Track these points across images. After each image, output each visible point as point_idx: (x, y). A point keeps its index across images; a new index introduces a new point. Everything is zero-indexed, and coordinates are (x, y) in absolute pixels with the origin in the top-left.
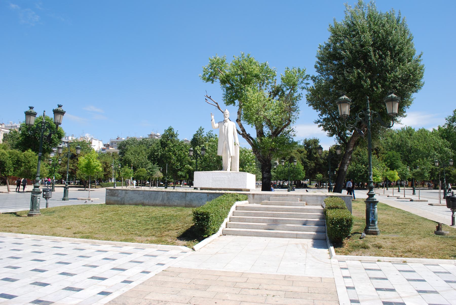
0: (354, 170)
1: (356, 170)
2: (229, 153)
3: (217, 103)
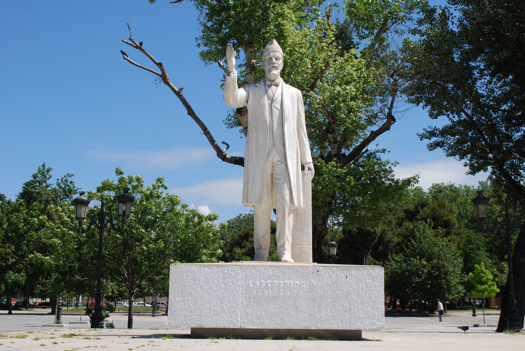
0: (403, 272)
1: (407, 271)
2: (287, 197)
3: (160, 65)
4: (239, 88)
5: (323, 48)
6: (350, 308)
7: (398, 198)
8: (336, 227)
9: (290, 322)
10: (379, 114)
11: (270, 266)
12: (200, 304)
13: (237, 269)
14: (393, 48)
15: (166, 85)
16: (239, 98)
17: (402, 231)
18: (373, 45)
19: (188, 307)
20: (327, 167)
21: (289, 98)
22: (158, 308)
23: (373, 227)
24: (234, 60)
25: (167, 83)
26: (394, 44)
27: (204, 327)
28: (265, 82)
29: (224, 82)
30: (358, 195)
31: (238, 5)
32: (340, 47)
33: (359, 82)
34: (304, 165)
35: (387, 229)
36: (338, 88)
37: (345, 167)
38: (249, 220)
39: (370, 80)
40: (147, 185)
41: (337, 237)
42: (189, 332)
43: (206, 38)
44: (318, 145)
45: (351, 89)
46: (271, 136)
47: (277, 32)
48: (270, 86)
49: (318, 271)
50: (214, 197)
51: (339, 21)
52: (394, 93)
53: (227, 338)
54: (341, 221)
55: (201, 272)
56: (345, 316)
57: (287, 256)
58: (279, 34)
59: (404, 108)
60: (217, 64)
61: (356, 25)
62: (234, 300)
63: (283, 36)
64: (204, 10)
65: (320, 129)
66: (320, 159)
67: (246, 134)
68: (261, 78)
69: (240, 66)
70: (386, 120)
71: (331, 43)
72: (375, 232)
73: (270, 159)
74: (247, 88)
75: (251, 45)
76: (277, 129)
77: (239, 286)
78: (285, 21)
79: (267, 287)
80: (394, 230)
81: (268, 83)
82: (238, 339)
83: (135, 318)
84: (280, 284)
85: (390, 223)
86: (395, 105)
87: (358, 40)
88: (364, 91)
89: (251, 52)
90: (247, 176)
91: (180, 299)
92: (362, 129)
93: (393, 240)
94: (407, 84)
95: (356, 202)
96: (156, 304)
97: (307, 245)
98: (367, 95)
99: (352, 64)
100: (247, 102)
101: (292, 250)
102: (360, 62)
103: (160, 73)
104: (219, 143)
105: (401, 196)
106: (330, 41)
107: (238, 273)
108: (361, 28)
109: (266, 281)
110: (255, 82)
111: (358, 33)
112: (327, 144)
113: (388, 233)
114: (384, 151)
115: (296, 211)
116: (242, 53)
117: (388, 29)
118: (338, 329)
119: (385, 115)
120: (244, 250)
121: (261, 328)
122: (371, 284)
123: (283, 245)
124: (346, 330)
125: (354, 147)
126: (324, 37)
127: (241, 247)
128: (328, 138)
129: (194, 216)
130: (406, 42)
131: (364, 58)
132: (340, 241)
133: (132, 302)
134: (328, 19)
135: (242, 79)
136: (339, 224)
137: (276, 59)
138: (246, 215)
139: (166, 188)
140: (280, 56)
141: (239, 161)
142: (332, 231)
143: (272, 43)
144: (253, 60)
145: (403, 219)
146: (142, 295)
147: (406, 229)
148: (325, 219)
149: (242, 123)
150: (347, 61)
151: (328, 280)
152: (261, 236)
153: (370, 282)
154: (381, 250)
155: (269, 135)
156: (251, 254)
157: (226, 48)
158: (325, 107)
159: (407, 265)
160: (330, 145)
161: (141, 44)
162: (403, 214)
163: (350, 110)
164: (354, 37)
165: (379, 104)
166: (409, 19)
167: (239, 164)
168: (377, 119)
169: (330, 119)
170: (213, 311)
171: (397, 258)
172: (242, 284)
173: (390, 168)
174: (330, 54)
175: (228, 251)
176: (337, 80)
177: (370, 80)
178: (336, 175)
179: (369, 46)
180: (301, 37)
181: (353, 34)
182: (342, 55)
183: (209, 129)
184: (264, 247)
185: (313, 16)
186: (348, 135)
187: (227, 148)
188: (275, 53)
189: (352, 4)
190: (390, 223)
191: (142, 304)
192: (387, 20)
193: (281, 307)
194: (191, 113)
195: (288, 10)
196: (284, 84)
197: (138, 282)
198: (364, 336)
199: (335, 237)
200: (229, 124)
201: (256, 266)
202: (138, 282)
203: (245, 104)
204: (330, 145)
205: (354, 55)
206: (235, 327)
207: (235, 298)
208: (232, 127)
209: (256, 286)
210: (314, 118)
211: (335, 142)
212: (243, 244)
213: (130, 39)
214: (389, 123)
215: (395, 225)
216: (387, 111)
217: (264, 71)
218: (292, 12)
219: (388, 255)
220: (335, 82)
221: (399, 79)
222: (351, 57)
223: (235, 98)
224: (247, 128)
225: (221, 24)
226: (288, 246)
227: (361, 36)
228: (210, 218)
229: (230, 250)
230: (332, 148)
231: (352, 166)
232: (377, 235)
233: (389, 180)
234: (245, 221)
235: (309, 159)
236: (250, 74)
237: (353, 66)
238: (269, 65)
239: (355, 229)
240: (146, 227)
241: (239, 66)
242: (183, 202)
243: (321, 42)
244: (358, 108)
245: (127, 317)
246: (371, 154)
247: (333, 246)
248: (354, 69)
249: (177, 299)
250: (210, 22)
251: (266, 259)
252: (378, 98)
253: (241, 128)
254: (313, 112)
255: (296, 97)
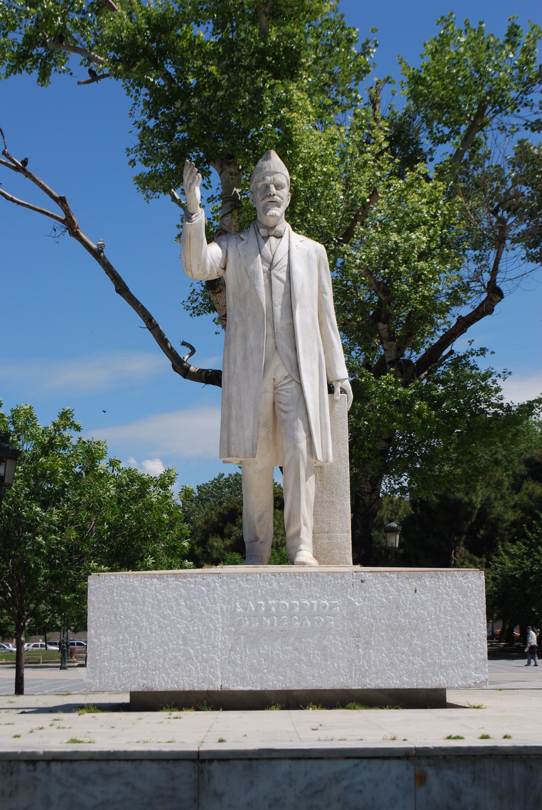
0: (526, 575)
1: (532, 573)
2: (303, 445)
3: (61, 201)
4: (208, 243)
5: (365, 163)
6: (424, 649)
7: (511, 439)
8: (397, 496)
9: (313, 676)
10: (472, 285)
11: (274, 574)
12: (145, 647)
13: (213, 580)
14: (496, 159)
15: (73, 240)
16: (209, 261)
17: (523, 500)
18: (459, 154)
19: (123, 653)
20: (378, 386)
21: (301, 259)
22: (72, 653)
23: (467, 494)
24: (198, 191)
25: (76, 235)
26: (497, 152)
27: (155, 689)
28: (257, 232)
29: (181, 230)
30: (437, 436)
31: (204, 85)
32: (397, 160)
33: (433, 225)
34: (334, 383)
35: (493, 496)
36: (394, 237)
37: (412, 385)
38: (235, 484)
39: (453, 220)
40: (45, 420)
41: (401, 512)
42: (126, 699)
43: (147, 149)
44: (360, 345)
45: (419, 237)
46: (271, 331)
47: (279, 134)
48: (266, 238)
49: (362, 581)
50: (171, 444)
51: (396, 111)
52: (499, 242)
53: (197, 709)
54: (405, 484)
55: (146, 587)
56: (414, 664)
57: (305, 554)
58: (283, 139)
59: (517, 273)
60: (169, 197)
61: (426, 116)
62: (209, 638)
63: (290, 142)
64: (141, 98)
65: (364, 313)
66: (364, 370)
67: (224, 327)
68: (250, 222)
69: (211, 199)
70: (485, 295)
71: (381, 153)
72: (470, 503)
73: (270, 375)
74: (224, 243)
75: (231, 161)
76: (282, 319)
77: (217, 612)
78: (295, 114)
79: (268, 613)
80: (507, 497)
81: (263, 232)
82: (218, 710)
83: (28, 674)
84: (292, 606)
85: (499, 484)
86: (501, 266)
87: (431, 146)
88: (444, 242)
89: (231, 174)
90: (227, 406)
91: (109, 639)
92: (442, 312)
93: (506, 516)
94: (524, 227)
95: (433, 448)
96: (68, 647)
97: (343, 532)
98: (447, 248)
99: (419, 191)
100: (225, 269)
101: (314, 542)
102: (435, 187)
103: (63, 217)
104: (175, 344)
105: (515, 435)
106: (378, 150)
107: (215, 589)
108: (435, 123)
109: (266, 601)
110: (241, 231)
111: (431, 132)
112: (377, 341)
113: (496, 504)
114: (483, 351)
115: (319, 471)
116: (215, 177)
117: (486, 123)
118: (403, 687)
119: (483, 285)
120: (228, 542)
121: (259, 689)
122: (462, 603)
123: (298, 534)
124: (416, 689)
125: (427, 346)
126: (368, 142)
127: (223, 536)
128: (377, 331)
129: (132, 481)
130: (523, 148)
131: (441, 180)
132: (406, 519)
133: (23, 644)
134: (375, 109)
135: (215, 223)
136: (403, 490)
137: (277, 187)
138: (230, 475)
139: (78, 429)
140: (285, 182)
141: (213, 378)
142: (391, 502)
143: (268, 158)
144: (235, 189)
145: (524, 477)
146: (41, 629)
147: (530, 496)
148: (376, 482)
149: (217, 307)
150: (410, 186)
151: (381, 596)
152: (256, 517)
153: (458, 599)
154: (483, 536)
155: (267, 330)
156: (239, 551)
157: (183, 166)
158: (370, 273)
159: (532, 563)
160: (381, 343)
161: (25, 162)
162: (523, 467)
163: (418, 277)
164: (424, 140)
165: (473, 266)
166: (526, 105)
167: (214, 384)
168: (469, 294)
169: (381, 295)
170: (171, 659)
171: (513, 549)
172: (222, 608)
173: (494, 382)
174: (378, 174)
175: (199, 544)
176: (392, 223)
177: (453, 220)
178: (395, 399)
179: (451, 155)
180: (324, 143)
181: (421, 135)
182: (401, 176)
183: (157, 318)
184: (261, 538)
185: (346, 101)
186: (418, 321)
187: (191, 355)
188: (275, 176)
189: (420, 78)
190: (499, 484)
191: (42, 646)
192: (485, 108)
193: (296, 649)
194: (122, 289)
195: (299, 94)
196: (294, 235)
197: (32, 606)
198: (450, 699)
199: (396, 514)
200: (194, 308)
201: (248, 574)
202: (32, 606)
203: (221, 273)
204: (381, 343)
205: (423, 175)
206: (211, 688)
207: (210, 634)
208: (198, 315)
209: (248, 612)
210: (352, 293)
211: (392, 337)
212: (226, 531)
213: (4, 153)
214: (492, 300)
215: (508, 489)
216: (486, 277)
217: (255, 209)
218: (306, 97)
219: (496, 546)
220: (389, 225)
221: (509, 217)
222: (417, 179)
223: (202, 263)
224: (225, 316)
225: (173, 121)
226: (306, 535)
227: (436, 138)
228: (164, 482)
229: (203, 543)
230: (385, 350)
231: (425, 381)
232: (474, 508)
233: (492, 405)
234: (229, 487)
235: (343, 372)
236: (230, 216)
237: (422, 195)
238: (263, 199)
239: (434, 498)
240: (45, 506)
241: (209, 200)
242: (111, 455)
243: (362, 153)
244: (432, 273)
245: (13, 672)
246: (459, 359)
247: (393, 530)
248: (424, 200)
249: (103, 639)
250: (153, 120)
251: (266, 560)
252: (471, 253)
253: (215, 315)
254: (350, 283)
255: (314, 256)
